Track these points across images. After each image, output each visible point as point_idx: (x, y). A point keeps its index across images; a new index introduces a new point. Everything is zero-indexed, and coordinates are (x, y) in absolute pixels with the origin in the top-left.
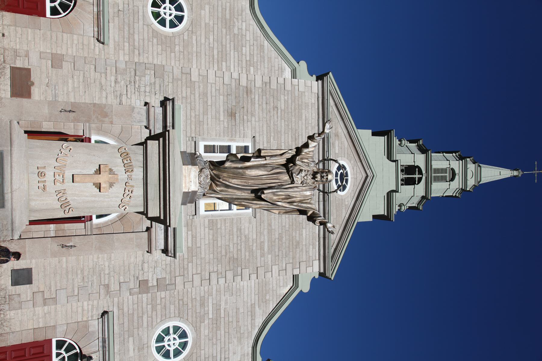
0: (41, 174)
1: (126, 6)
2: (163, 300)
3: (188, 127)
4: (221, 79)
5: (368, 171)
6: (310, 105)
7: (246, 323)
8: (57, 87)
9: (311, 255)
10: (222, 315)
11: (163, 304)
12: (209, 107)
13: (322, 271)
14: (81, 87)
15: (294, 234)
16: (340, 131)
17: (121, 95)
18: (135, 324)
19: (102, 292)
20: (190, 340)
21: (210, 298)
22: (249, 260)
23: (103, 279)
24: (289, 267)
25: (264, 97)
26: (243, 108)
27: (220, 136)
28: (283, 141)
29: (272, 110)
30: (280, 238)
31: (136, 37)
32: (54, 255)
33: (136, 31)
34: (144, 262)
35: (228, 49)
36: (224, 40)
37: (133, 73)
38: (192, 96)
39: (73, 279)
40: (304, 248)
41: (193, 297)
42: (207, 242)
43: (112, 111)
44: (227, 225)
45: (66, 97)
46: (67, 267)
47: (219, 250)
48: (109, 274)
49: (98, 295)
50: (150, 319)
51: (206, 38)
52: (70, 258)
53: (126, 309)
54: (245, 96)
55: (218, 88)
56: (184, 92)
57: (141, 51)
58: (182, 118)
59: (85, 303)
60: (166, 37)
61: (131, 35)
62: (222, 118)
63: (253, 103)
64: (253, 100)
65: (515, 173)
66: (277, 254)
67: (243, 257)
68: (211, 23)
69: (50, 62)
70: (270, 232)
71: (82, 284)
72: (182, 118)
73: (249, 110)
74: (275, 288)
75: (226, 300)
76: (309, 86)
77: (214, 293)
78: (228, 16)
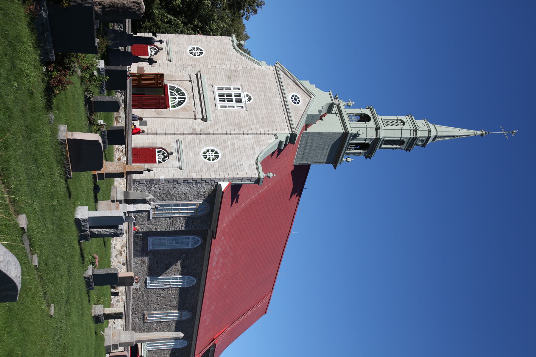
16: (290, 83)
53: (187, 140)
58: (206, 79)
62: (224, 78)
63: (239, 74)
70: (256, 116)
72: (206, 79)
78: (223, 51)
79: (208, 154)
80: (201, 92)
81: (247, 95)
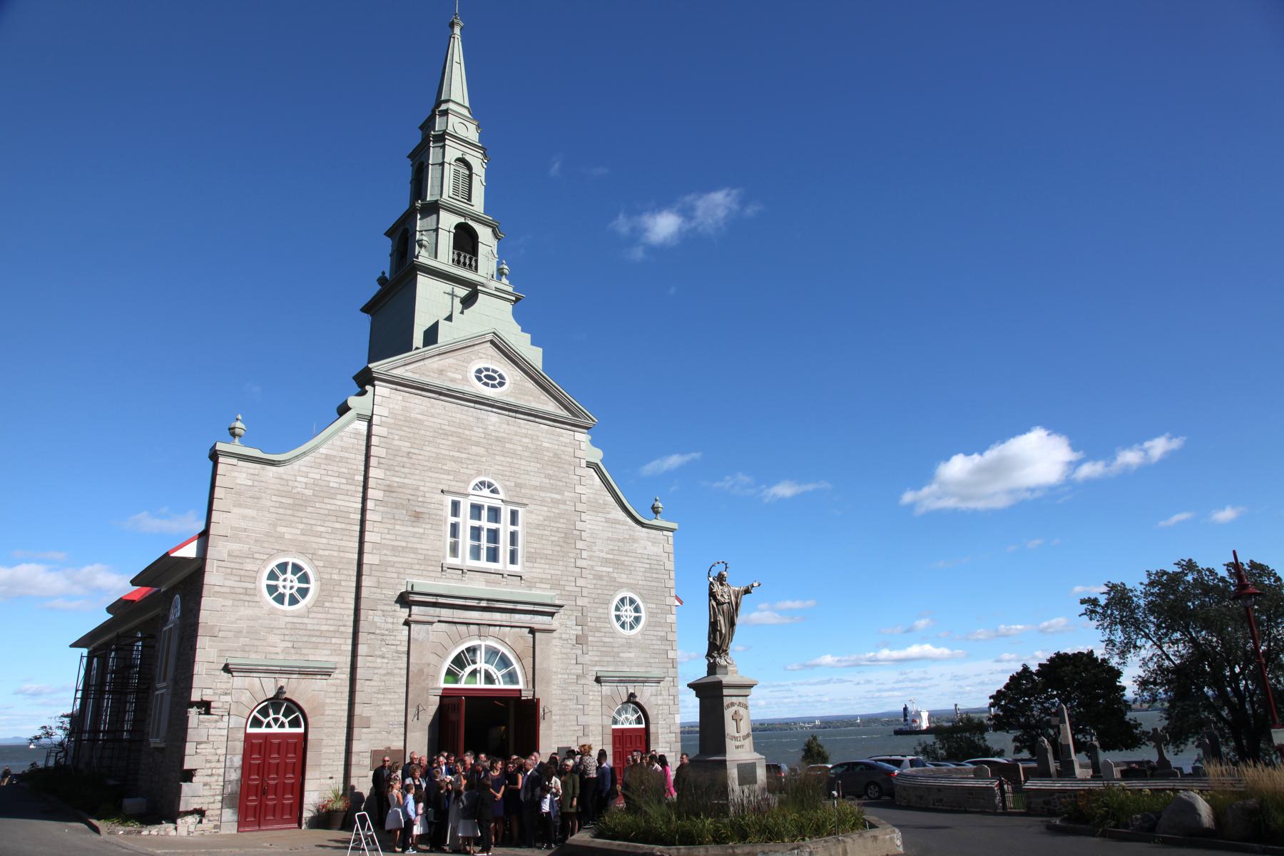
16: (435, 366)
17: (397, 652)
19: (582, 682)
31: (324, 628)
33: (316, 627)
60: (322, 590)
61: (321, 634)
62: (421, 530)
63: (402, 486)
68: (301, 526)
70: (541, 488)
78: (290, 501)
80: (484, 604)
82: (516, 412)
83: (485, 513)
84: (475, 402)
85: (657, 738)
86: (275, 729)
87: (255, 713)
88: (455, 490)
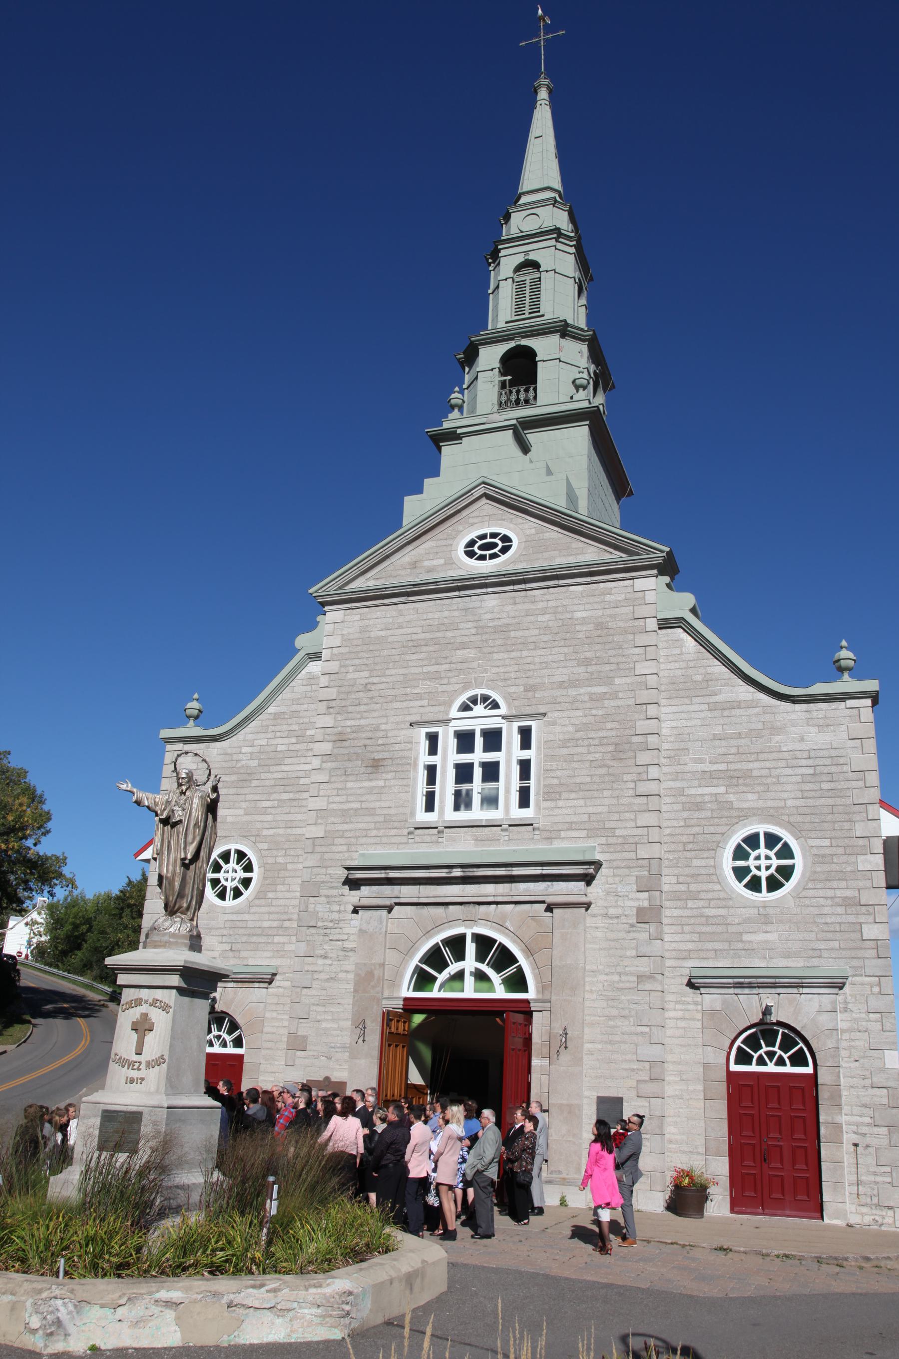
0: (132, 1081)
1: (225, 939)
2: (681, 879)
3: (393, 840)
4: (322, 786)
5: (477, 495)
6: (362, 623)
7: (745, 719)
8: (332, 1045)
9: (623, 597)
10: (723, 767)
11: (689, 880)
12: (364, 806)
13: (655, 572)
14: (332, 1010)
15: (581, 635)
16: (407, 559)
17: (344, 949)
18: (720, 929)
19: (648, 986)
20: (761, 828)
21: (687, 792)
22: (620, 722)
23: (628, 985)
24: (642, 640)
25: (350, 709)
26: (365, 746)
27: (408, 786)
28: (420, 670)
29: (370, 694)
30: (586, 662)
31: (266, 924)
32: (578, 1061)
33: (258, 924)
34: (606, 915)
35: (280, 775)
36: (267, 783)
37: (313, 931)
38: (346, 834)
39: (623, 1033)
40: (608, 612)
41: (682, 824)
42: (582, 802)
43: (365, 964)
44: (555, 767)
45: (345, 1033)
46: (601, 1042)
47: (597, 779)
48: (620, 974)
49: (653, 993)
50: (713, 903)
51: (265, 814)
52: (586, 1037)
53: (690, 946)
54: (347, 744)
55: (335, 792)
56: (340, 848)
57: (285, 917)
58: (379, 850)
59: (671, 1014)
60: (265, 878)
62: (381, 783)
63: (358, 729)
64: (354, 728)
65: (543, 94)
66: (614, 667)
67: (614, 733)
68: (244, 805)
69: (299, 1053)
70: (574, 683)
71: (631, 1019)
72: (379, 850)
73: (370, 735)
74: (683, 665)
75: (695, 761)
76: (335, 627)
77: (678, 784)
79: (230, 885)
80: (457, 873)
81: (465, 708)
82: (525, 581)
83: (479, 741)
84: (459, 589)
85: (836, 1098)
86: (771, 1068)
87: (738, 1043)
88: (431, 717)
